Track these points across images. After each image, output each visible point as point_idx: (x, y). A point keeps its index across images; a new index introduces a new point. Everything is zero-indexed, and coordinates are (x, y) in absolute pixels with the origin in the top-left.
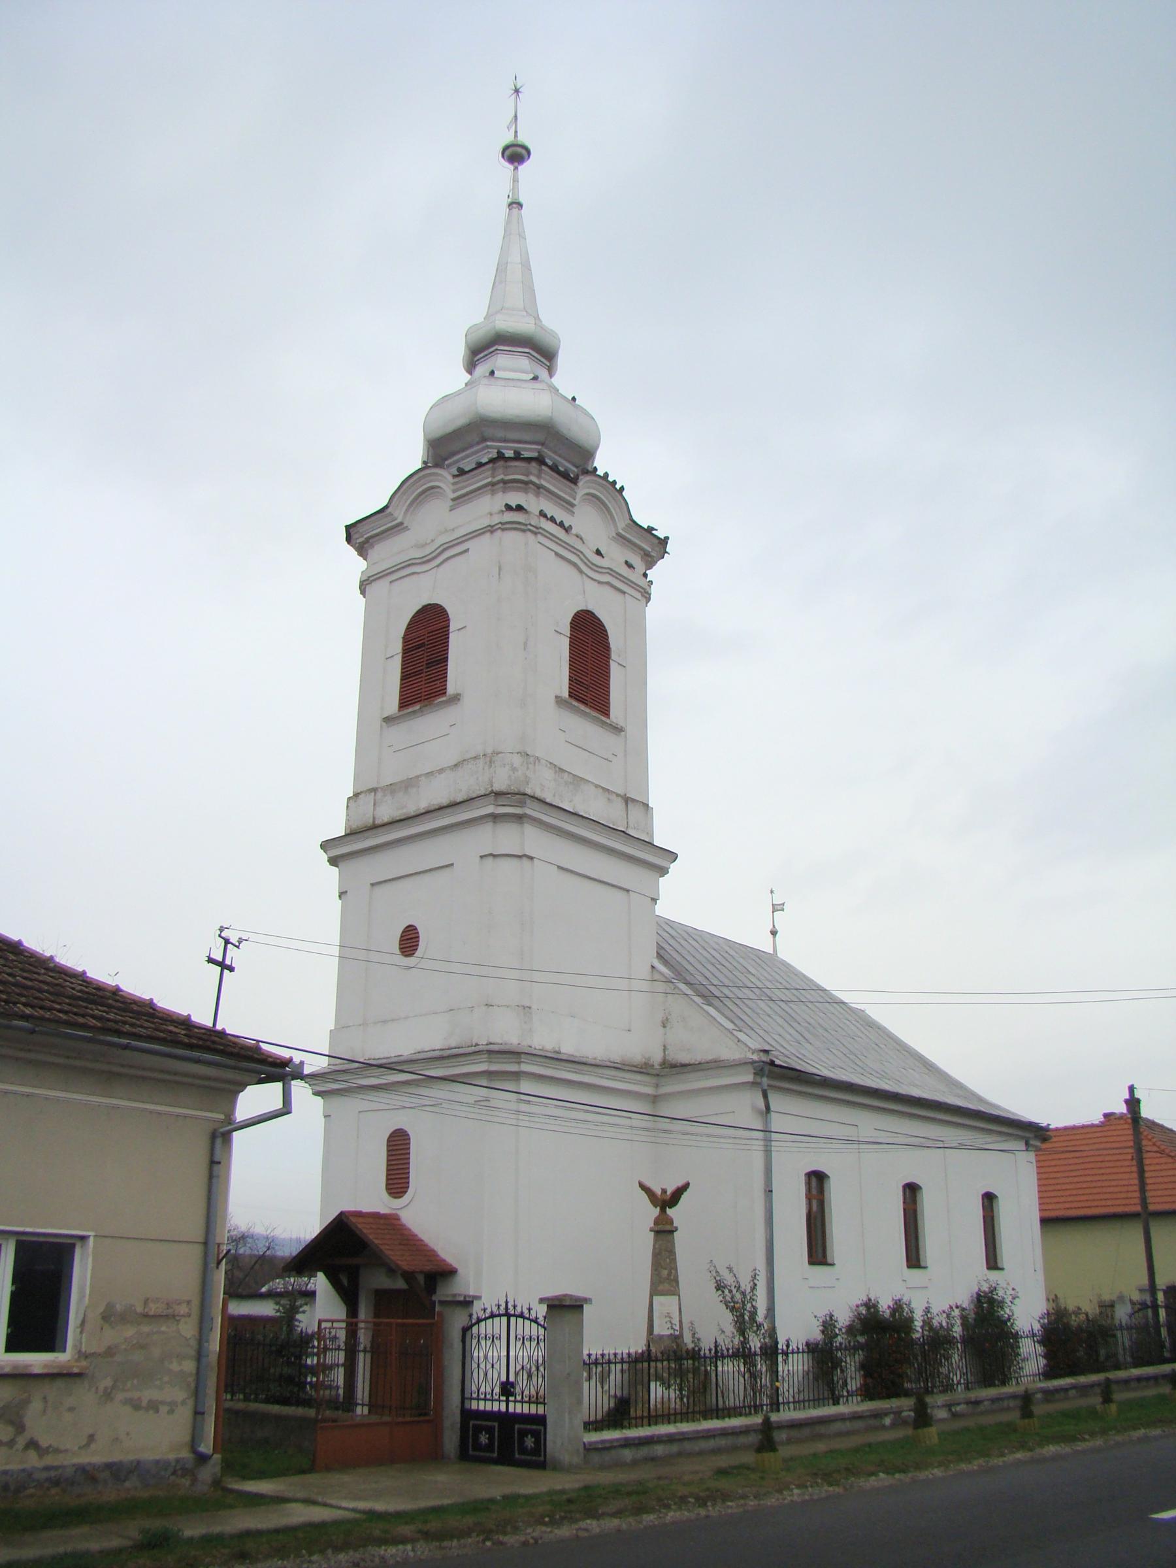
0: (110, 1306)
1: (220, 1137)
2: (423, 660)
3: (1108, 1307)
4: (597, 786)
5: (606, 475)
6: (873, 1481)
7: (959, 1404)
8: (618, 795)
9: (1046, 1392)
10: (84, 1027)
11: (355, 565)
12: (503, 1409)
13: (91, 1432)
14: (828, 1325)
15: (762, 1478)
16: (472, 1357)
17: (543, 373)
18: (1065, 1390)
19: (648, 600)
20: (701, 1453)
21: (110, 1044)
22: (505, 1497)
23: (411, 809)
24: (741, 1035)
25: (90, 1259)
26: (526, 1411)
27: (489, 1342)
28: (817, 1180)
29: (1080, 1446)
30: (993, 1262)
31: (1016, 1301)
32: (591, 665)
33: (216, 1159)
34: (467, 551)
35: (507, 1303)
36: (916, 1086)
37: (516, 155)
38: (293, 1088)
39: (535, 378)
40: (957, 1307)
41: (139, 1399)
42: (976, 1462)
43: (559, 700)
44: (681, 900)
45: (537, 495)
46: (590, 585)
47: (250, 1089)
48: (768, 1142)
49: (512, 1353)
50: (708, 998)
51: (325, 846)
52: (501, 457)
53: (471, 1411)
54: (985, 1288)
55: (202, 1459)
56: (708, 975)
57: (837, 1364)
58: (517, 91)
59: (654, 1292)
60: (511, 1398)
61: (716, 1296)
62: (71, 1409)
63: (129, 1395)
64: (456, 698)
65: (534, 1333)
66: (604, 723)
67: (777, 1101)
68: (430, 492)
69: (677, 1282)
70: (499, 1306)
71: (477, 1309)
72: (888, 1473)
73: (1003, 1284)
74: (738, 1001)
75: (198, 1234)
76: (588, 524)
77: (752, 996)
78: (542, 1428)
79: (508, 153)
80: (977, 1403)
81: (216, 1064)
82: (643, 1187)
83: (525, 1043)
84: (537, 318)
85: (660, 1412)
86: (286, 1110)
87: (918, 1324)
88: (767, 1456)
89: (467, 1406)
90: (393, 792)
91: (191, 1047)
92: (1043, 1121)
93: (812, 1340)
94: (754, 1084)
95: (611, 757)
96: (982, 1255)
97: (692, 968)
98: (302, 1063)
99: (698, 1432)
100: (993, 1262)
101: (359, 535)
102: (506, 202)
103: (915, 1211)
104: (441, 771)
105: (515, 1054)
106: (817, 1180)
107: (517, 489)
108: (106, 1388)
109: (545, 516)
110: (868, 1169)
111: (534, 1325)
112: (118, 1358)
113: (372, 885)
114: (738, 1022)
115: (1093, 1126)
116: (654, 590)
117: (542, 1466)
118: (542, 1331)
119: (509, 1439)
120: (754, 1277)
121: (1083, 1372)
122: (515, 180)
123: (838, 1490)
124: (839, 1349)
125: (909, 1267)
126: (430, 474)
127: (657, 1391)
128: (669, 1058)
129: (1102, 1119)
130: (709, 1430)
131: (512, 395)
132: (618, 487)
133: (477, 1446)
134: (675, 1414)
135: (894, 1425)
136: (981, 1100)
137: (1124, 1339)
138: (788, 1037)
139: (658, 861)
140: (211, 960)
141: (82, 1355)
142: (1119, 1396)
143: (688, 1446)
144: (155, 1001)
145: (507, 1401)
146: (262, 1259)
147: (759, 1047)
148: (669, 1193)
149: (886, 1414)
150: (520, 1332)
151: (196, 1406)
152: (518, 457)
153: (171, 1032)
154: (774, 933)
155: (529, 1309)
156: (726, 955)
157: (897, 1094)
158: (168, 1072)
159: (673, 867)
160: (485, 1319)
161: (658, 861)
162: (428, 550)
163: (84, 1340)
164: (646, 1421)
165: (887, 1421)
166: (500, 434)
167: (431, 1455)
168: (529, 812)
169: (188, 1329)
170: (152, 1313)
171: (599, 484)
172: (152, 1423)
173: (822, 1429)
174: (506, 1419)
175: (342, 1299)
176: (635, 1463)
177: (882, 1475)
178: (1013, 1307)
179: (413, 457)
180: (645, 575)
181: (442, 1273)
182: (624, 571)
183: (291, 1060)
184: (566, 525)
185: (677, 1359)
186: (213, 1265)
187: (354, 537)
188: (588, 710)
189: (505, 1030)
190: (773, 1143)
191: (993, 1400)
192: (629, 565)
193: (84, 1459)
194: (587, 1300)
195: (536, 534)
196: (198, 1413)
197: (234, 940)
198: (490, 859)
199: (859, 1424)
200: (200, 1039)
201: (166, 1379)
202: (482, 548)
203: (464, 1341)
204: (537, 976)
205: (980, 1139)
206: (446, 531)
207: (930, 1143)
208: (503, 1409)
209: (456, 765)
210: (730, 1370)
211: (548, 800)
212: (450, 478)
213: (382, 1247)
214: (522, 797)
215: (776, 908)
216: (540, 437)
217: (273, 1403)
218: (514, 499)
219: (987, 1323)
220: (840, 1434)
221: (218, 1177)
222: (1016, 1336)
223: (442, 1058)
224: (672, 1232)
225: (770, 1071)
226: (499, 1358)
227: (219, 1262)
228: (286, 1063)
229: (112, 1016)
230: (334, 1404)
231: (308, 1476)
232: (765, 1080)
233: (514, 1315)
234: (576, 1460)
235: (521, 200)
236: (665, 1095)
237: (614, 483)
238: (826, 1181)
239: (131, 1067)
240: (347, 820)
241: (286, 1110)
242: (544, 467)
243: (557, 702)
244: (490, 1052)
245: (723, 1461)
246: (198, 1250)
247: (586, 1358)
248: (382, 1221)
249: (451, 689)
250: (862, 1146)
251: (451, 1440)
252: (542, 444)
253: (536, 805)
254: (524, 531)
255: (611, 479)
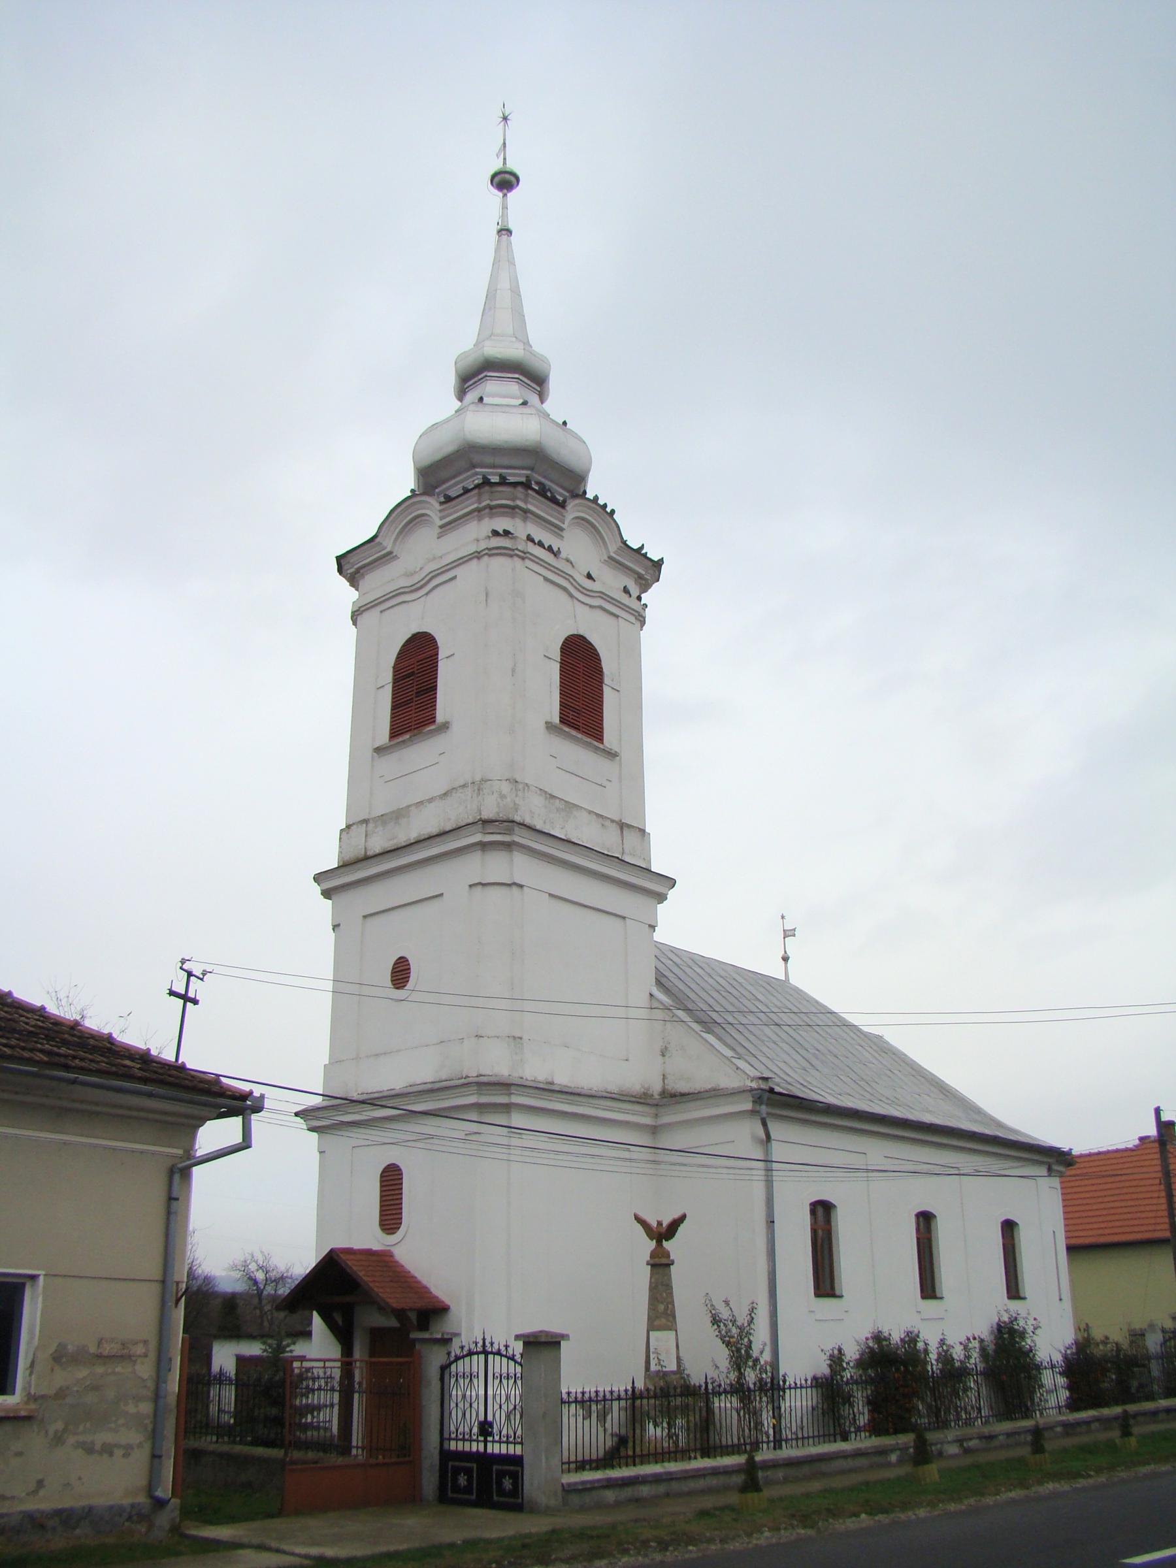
0: (62, 1347)
1: (179, 1173)
2: (413, 689)
3: (1137, 1336)
4: (590, 812)
5: (596, 498)
6: (850, 1524)
7: (971, 1439)
8: (613, 821)
9: (1065, 1425)
10: (30, 1061)
11: (347, 595)
12: (482, 1449)
13: (40, 1477)
14: (836, 1359)
15: (735, 1520)
16: (450, 1396)
17: (534, 399)
18: (1087, 1423)
19: (643, 623)
20: (690, 1493)
21: (53, 1078)
22: (466, 1542)
23: (402, 838)
24: (741, 1064)
25: (40, 1299)
26: (504, 1451)
27: (467, 1381)
28: (822, 1211)
29: (1081, 1483)
30: (1014, 1291)
31: (1037, 1332)
32: (583, 690)
33: (175, 1195)
34: (455, 577)
35: (484, 1340)
36: (929, 1112)
37: (505, 181)
38: (253, 1123)
39: (525, 403)
40: (974, 1338)
41: (93, 1443)
42: (966, 1502)
43: (549, 726)
44: (680, 925)
45: (525, 519)
46: (582, 610)
47: (210, 1124)
48: (769, 1170)
49: (490, 1392)
50: (708, 1025)
51: (318, 878)
52: (486, 482)
53: (450, 1452)
54: (1005, 1318)
55: (160, 1504)
56: (711, 1001)
57: (848, 1399)
58: (505, 119)
59: (652, 1326)
60: (490, 1439)
61: (711, 1331)
62: (19, 1454)
63: (81, 1438)
64: (445, 726)
65: (512, 1370)
66: (597, 748)
67: (777, 1130)
68: (418, 520)
69: (674, 1317)
70: (476, 1343)
71: (455, 1349)
72: (871, 1514)
73: (1023, 1314)
74: (741, 1028)
75: (156, 1273)
76: (578, 549)
77: (757, 1021)
78: (519, 1469)
79: (497, 180)
80: (991, 1437)
81: (177, 1100)
82: (638, 1219)
83: (516, 1074)
84: (527, 344)
85: (666, 1450)
86: (246, 1144)
87: (933, 1356)
88: (752, 1497)
89: (446, 1446)
90: (384, 823)
91: (145, 1081)
92: (1065, 1147)
93: (819, 1375)
94: (753, 1112)
95: (605, 783)
96: (1001, 1284)
97: (691, 995)
98: (262, 1096)
99: (686, 1471)
100: (1014, 1291)
101: (351, 566)
102: (495, 228)
103: (930, 1240)
104: (431, 800)
105: (505, 1086)
106: (822, 1211)
107: (503, 515)
108: (56, 1432)
109: (532, 541)
110: (877, 1200)
111: (512, 1363)
112: (69, 1400)
113: (365, 917)
114: (739, 1049)
115: (1127, 1150)
116: (648, 613)
117: (518, 1508)
118: (519, 1369)
119: (487, 1480)
120: (752, 1310)
121: (1107, 1405)
122: (505, 207)
123: (810, 1532)
124: (847, 1383)
125: (923, 1297)
126: (420, 502)
127: (654, 1432)
128: (669, 1087)
129: (1137, 1142)
130: (699, 1470)
131: (502, 420)
132: (608, 510)
133: (456, 1488)
134: (669, 1453)
135: (900, 1461)
136: (999, 1125)
137: (1155, 1369)
138: (793, 1064)
139: (657, 887)
140: (172, 993)
141: (31, 1398)
142: (1136, 1430)
143: (675, 1486)
144: (115, 1035)
145: (486, 1442)
146: (996, 1338)
147: (759, 1074)
148: (665, 1224)
149: (892, 1451)
150: (497, 1370)
151: (153, 1448)
152: (503, 482)
153: (125, 1066)
154: (785, 959)
155: (507, 1347)
156: (732, 982)
157: (907, 1120)
158: (121, 1107)
159: (671, 894)
160: (464, 1357)
161: (657, 887)
162: (416, 578)
163: (33, 1382)
164: (630, 1461)
165: (893, 1458)
166: (489, 460)
167: (410, 1498)
168: (517, 839)
169: (145, 1369)
170: (106, 1353)
171: (590, 508)
172: (110, 1470)
173: (824, 1467)
174: (485, 1460)
175: (336, 1336)
176: (618, 1504)
177: (863, 1516)
178: (1035, 1337)
179: (404, 483)
180: (639, 598)
181: (431, 1312)
182: (624, 599)
183: (251, 1093)
184: (555, 549)
185: (670, 1395)
186: (171, 1304)
187: (345, 568)
188: (580, 736)
189: (496, 1062)
190: (774, 1173)
191: (1008, 1435)
192: (626, 590)
193: (31, 1506)
194: (565, 1337)
195: (523, 559)
196: (155, 1456)
197: (198, 972)
198: (479, 888)
199: (862, 1462)
200: (156, 1072)
201: (121, 1421)
202: (469, 574)
203: (442, 1379)
204: (528, 1006)
205: (996, 1165)
206: (434, 558)
207: (937, 1170)
208: (482, 1449)
209: (445, 794)
210: (725, 1405)
211: (538, 827)
212: (437, 506)
213: (371, 1285)
214: (509, 824)
215: (788, 934)
216: (528, 462)
217: (258, 1445)
218: (501, 524)
219: (1008, 1355)
220: (843, 1472)
221: (176, 1213)
222: (1038, 1367)
223: (432, 1091)
224: (668, 1265)
225: (769, 1099)
226: (477, 1396)
227: (178, 1300)
228: (245, 1096)
229: (63, 1050)
230: (324, 1446)
231: (275, 1520)
232: (763, 1107)
233: (492, 1353)
234: (553, 1502)
235: (511, 227)
236: (670, 1124)
237: (605, 506)
238: (1015, 1230)
239: (82, 1102)
240: (340, 852)
241: (246, 1144)
242: (530, 492)
243: (547, 728)
244: (479, 1084)
245: (708, 1502)
246: (156, 1288)
247: (565, 1396)
248: (374, 1258)
249: (440, 717)
250: (870, 1174)
251: (429, 1482)
252: (532, 469)
253: (524, 832)
254: (511, 556)
255: (601, 502)
